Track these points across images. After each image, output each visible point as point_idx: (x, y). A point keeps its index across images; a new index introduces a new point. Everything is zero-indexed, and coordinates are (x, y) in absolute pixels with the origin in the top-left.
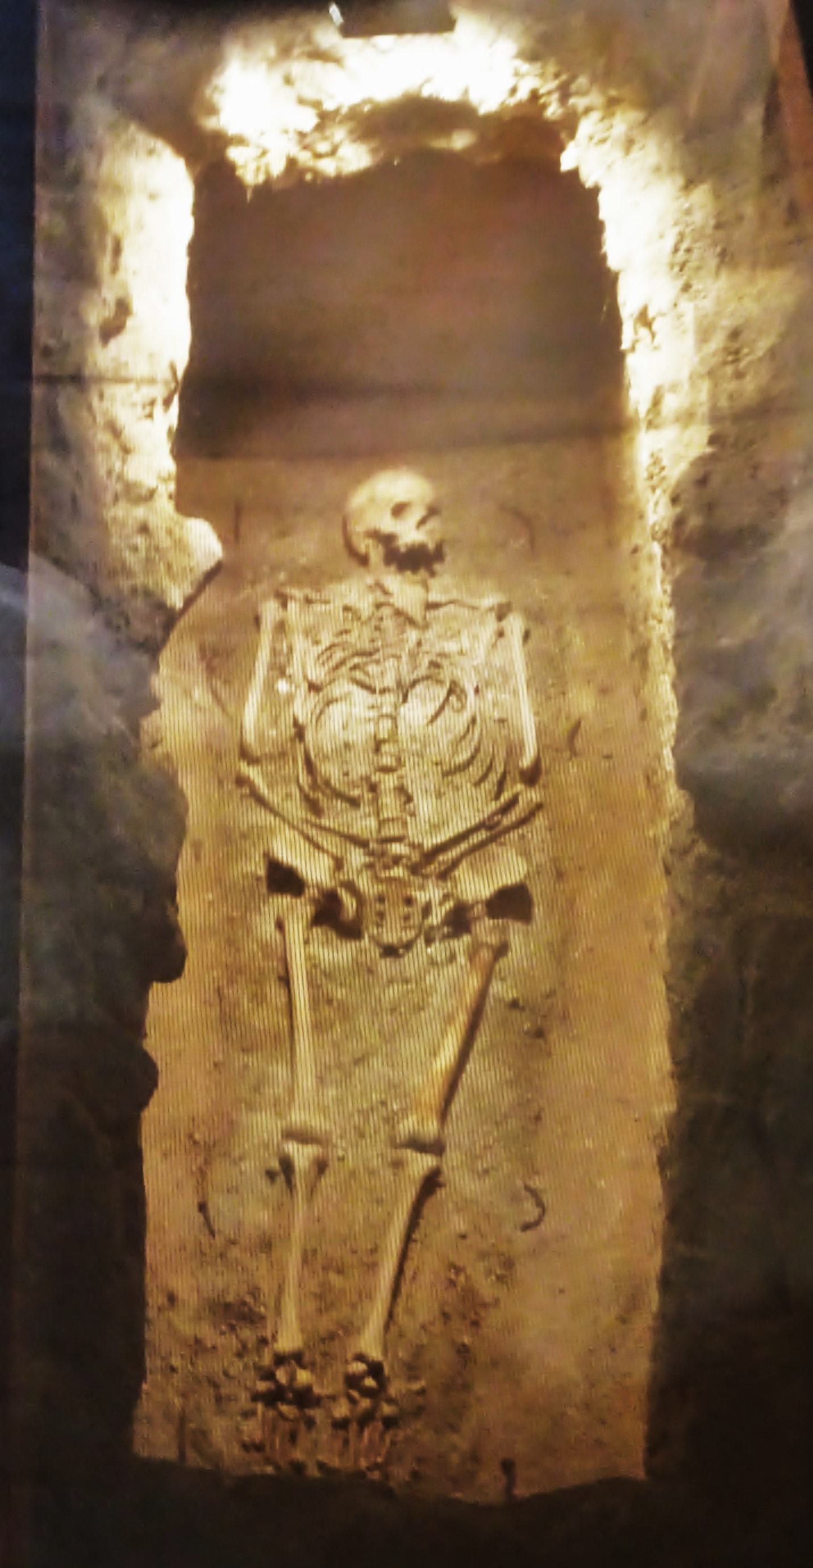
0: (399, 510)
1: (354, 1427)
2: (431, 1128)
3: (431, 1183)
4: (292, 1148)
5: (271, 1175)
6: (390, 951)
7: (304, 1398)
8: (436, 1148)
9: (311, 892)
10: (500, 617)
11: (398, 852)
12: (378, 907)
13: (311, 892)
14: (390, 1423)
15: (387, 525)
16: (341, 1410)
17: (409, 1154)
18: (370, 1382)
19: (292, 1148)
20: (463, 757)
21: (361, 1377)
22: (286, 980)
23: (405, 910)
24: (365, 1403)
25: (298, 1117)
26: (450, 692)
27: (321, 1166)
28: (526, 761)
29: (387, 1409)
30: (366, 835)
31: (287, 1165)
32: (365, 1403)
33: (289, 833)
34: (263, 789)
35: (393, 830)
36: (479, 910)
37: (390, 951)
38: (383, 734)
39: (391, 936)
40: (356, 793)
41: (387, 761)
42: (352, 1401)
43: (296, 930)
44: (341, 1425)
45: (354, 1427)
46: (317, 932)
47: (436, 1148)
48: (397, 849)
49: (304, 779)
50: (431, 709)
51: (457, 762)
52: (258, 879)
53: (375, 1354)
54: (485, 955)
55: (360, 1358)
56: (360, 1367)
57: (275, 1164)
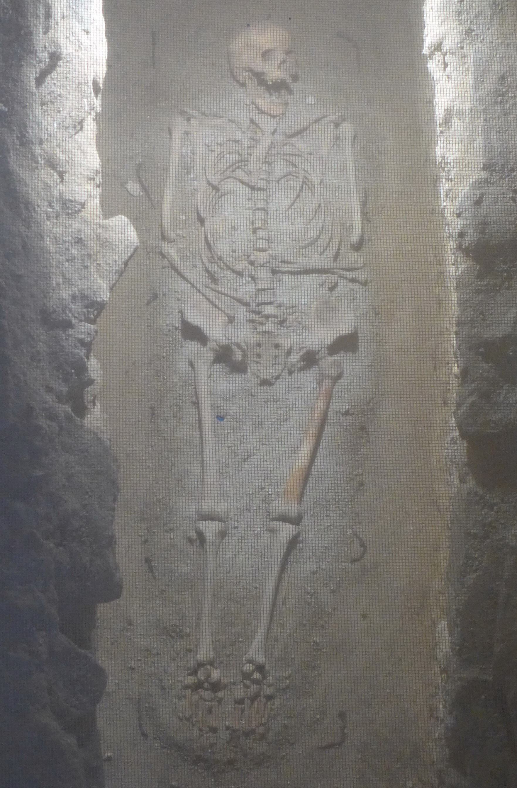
0: (266, 54)
1: (247, 702)
2: (293, 509)
3: (293, 542)
4: (203, 525)
5: (191, 541)
6: (265, 383)
7: (216, 687)
8: (297, 520)
9: (212, 344)
10: (337, 125)
11: (214, 725)
12: (257, 350)
13: (212, 344)
14: (269, 698)
15: (259, 66)
16: (239, 693)
17: (280, 525)
18: (257, 676)
19: (203, 525)
20: (313, 233)
21: (252, 673)
22: (196, 404)
23: (275, 352)
24: (254, 688)
25: (206, 506)
26: (304, 183)
27: (223, 534)
28: (355, 239)
29: (268, 691)
30: (247, 299)
31: (201, 535)
32: (254, 688)
33: (198, 297)
34: (178, 263)
35: (264, 297)
36: (325, 351)
37: (265, 383)
38: (258, 224)
39: (267, 373)
40: (239, 267)
41: (261, 244)
42: (246, 687)
43: (203, 370)
44: (240, 701)
45: (247, 702)
46: (217, 367)
47: (297, 520)
48: (269, 310)
49: (205, 254)
50: (293, 195)
51: (236, 696)
52: (176, 328)
53: (260, 659)
54: (327, 383)
55: (249, 661)
56: (249, 667)
57: (193, 534)
